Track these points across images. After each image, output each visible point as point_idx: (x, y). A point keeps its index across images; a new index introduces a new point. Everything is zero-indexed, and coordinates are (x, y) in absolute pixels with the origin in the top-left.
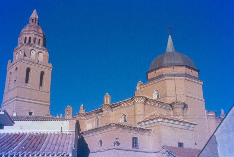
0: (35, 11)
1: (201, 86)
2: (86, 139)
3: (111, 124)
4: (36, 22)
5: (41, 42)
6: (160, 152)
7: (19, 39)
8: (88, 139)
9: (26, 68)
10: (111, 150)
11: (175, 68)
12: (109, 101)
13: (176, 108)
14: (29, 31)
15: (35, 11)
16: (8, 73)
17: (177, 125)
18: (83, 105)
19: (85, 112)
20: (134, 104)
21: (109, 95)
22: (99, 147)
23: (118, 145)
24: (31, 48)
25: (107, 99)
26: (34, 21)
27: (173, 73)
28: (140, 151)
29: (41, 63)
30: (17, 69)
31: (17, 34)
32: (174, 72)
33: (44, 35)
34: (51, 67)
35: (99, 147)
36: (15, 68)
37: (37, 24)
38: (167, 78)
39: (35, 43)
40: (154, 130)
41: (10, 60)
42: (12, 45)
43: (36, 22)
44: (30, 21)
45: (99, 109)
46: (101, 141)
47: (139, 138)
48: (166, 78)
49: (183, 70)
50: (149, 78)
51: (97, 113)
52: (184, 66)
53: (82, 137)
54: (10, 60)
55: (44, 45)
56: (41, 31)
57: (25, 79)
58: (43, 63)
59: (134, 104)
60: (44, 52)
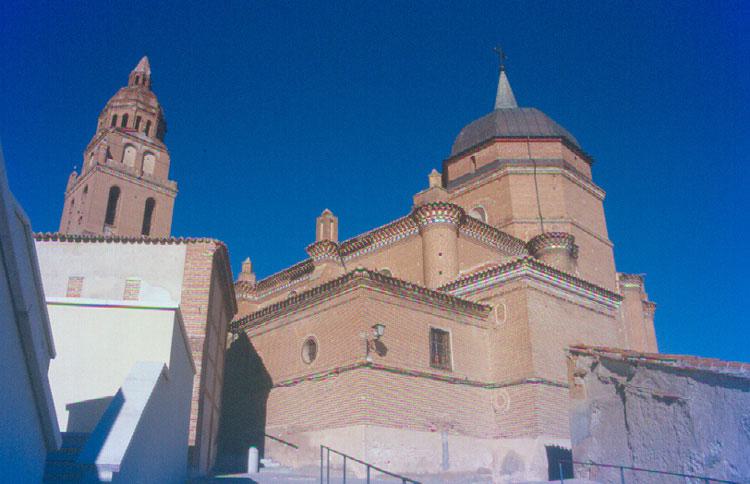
0: (145, 59)
1: (600, 202)
2: (255, 343)
3: (353, 272)
4: (144, 83)
5: (153, 128)
6: (528, 382)
7: (100, 121)
8: (262, 341)
9: (110, 186)
10: (353, 372)
11: (532, 144)
12: (334, 234)
13: (549, 252)
14: (126, 99)
15: (145, 59)
16: (68, 203)
17: (575, 296)
18: (251, 259)
19: (257, 279)
20: (421, 233)
21: (334, 215)
22: (304, 362)
23: (380, 355)
24: (125, 140)
25: (327, 228)
26: (140, 81)
27: (528, 157)
28: (455, 379)
29: (149, 179)
30: (86, 189)
31: (98, 109)
32: (529, 154)
33: (160, 112)
34: (174, 189)
35: (304, 362)
36: (83, 186)
37: (145, 89)
38: (512, 169)
39: (137, 127)
40: (501, 309)
41: (75, 172)
42: (84, 135)
43: (144, 83)
44: (132, 80)
45: (302, 265)
46: (311, 343)
47: (451, 335)
48: (509, 169)
49: (556, 150)
50: (451, 177)
51: (293, 279)
52: (558, 137)
53: (244, 338)
54: (75, 172)
55: (161, 134)
56: (154, 103)
57: (105, 213)
58: (155, 178)
59: (421, 233)
60: (158, 154)
